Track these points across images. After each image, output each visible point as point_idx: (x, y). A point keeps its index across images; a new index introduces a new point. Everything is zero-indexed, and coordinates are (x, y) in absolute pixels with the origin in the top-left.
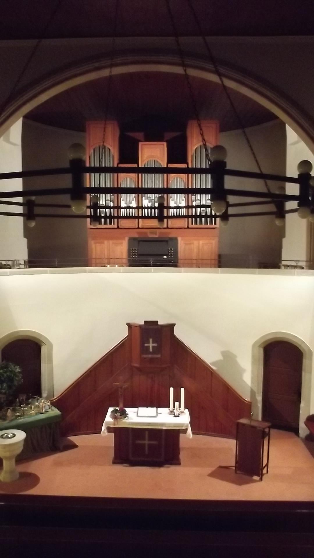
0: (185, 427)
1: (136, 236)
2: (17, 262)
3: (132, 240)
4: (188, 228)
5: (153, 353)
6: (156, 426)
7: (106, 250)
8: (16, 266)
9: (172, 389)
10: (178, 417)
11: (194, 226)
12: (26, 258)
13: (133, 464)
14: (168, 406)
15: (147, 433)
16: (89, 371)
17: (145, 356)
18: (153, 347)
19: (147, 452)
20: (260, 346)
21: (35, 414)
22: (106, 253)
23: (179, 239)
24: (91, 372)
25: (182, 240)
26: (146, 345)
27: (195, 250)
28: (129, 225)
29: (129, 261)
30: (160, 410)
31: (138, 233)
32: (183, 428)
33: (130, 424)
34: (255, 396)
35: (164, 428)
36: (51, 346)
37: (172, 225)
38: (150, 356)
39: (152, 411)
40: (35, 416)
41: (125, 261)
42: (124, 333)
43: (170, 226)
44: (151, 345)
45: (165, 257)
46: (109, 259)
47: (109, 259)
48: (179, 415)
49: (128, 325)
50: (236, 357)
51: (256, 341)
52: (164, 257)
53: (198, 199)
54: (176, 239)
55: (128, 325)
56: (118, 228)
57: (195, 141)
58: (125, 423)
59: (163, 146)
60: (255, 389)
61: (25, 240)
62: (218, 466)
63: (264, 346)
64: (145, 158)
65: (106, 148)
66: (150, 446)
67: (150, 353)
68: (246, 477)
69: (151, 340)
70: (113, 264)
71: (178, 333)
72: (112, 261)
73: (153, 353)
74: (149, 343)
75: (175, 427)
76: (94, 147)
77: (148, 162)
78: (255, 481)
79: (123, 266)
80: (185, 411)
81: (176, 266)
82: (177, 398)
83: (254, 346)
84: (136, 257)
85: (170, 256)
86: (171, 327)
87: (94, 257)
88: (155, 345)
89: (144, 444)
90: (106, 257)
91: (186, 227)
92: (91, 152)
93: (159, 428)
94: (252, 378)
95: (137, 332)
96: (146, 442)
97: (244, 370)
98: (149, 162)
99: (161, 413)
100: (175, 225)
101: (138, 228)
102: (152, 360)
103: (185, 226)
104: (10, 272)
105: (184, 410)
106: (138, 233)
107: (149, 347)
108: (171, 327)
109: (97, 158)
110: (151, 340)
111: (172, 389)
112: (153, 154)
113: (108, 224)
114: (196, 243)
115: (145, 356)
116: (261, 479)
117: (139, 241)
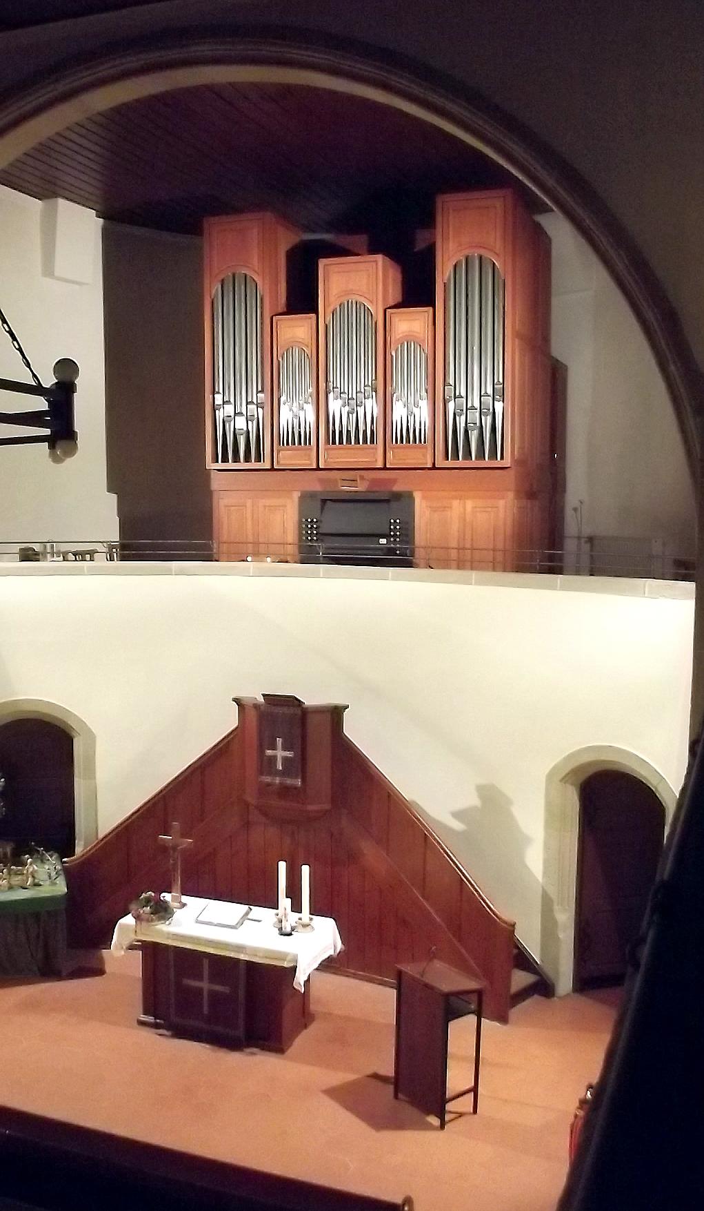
0: (290, 961)
1: (318, 488)
2: (52, 547)
3: (306, 498)
4: (434, 468)
5: (284, 773)
6: (222, 949)
7: (249, 522)
8: (49, 555)
9: (282, 866)
10: (290, 934)
11: (450, 463)
12: (114, 536)
13: (181, 1033)
14: (275, 906)
15: (206, 962)
16: (151, 803)
17: (268, 779)
18: (285, 759)
19: (206, 1010)
20: (564, 780)
21: (7, 889)
22: (250, 532)
23: (417, 496)
24: (155, 804)
25: (424, 498)
26: (269, 752)
27: (455, 527)
28: (298, 462)
29: (301, 549)
30: (257, 912)
31: (321, 481)
32: (286, 965)
33: (171, 936)
34: (551, 910)
35: (242, 957)
36: (92, 737)
37: (395, 461)
38: (277, 780)
39: (231, 911)
40: (6, 891)
41: (292, 550)
42: (229, 721)
43: (391, 464)
44: (280, 754)
45: (383, 541)
46: (256, 544)
47: (256, 544)
48: (293, 929)
49: (236, 700)
50: (509, 802)
51: (554, 768)
52: (381, 540)
53: (460, 393)
54: (410, 497)
55: (236, 700)
56: (272, 469)
57: (452, 245)
58: (161, 933)
59: (374, 264)
60: (553, 893)
61: (113, 498)
62: (370, 1071)
63: (583, 777)
64: (332, 299)
65: (248, 277)
66: (214, 996)
67: (277, 773)
68: (410, 1111)
69: (279, 741)
70: (258, 555)
71: (353, 730)
72: (262, 548)
73: (284, 773)
74: (274, 748)
75: (266, 957)
76: (222, 276)
77: (342, 305)
78: (430, 1127)
79: (287, 562)
80: (313, 923)
81: (408, 564)
82: (294, 892)
83: (550, 777)
84: (398, 540)
85: (392, 539)
86: (336, 713)
87: (225, 538)
88: (289, 754)
89: (200, 990)
90: (454, 544)
91: (380, 465)
92: (214, 292)
93: (232, 955)
94: (546, 863)
95: (252, 716)
96: (205, 985)
97: (527, 840)
98: (344, 306)
99: (260, 919)
100: (407, 461)
101: (318, 469)
102: (285, 791)
103: (426, 464)
104: (88, 567)
105: (311, 919)
106: (321, 481)
107: (275, 757)
108: (336, 713)
109: (228, 305)
110: (279, 741)
111: (282, 866)
112: (351, 287)
113: (253, 461)
114: (456, 503)
115: (268, 779)
116: (442, 1126)
117: (324, 501)
